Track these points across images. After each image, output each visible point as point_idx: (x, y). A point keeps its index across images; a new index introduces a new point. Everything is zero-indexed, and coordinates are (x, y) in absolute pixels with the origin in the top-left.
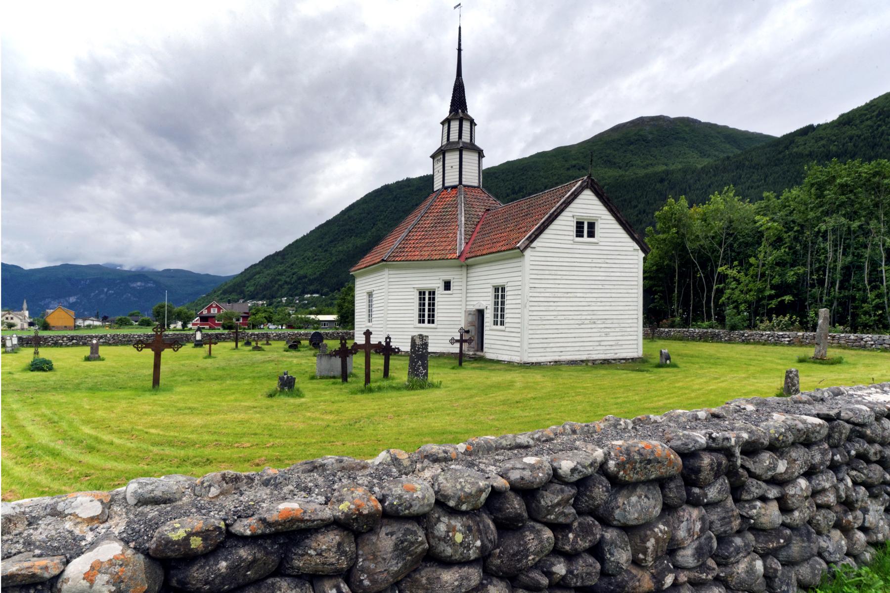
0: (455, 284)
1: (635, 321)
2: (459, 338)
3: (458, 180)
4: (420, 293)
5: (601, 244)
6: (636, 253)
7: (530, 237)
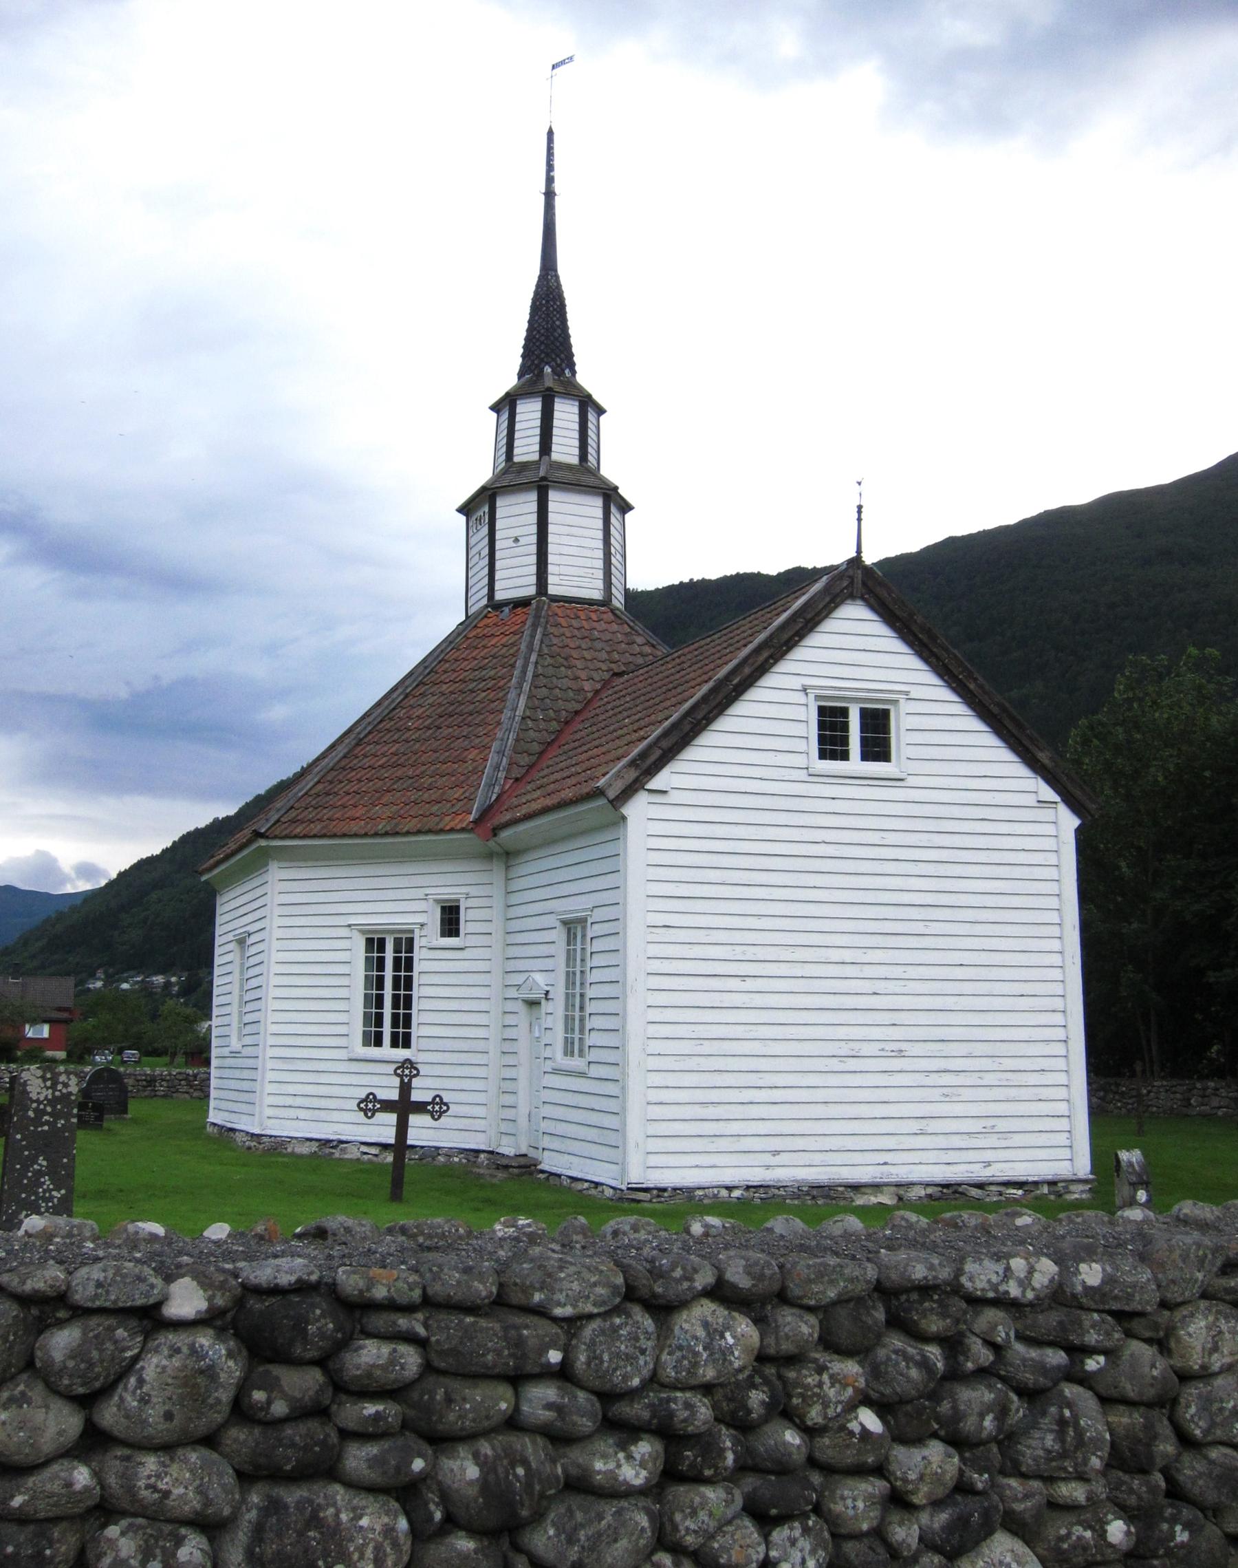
0: (472, 915)
1: (1060, 1049)
2: (394, 1095)
3: (533, 579)
4: (370, 942)
5: (911, 781)
6: (1048, 814)
7: (643, 755)
